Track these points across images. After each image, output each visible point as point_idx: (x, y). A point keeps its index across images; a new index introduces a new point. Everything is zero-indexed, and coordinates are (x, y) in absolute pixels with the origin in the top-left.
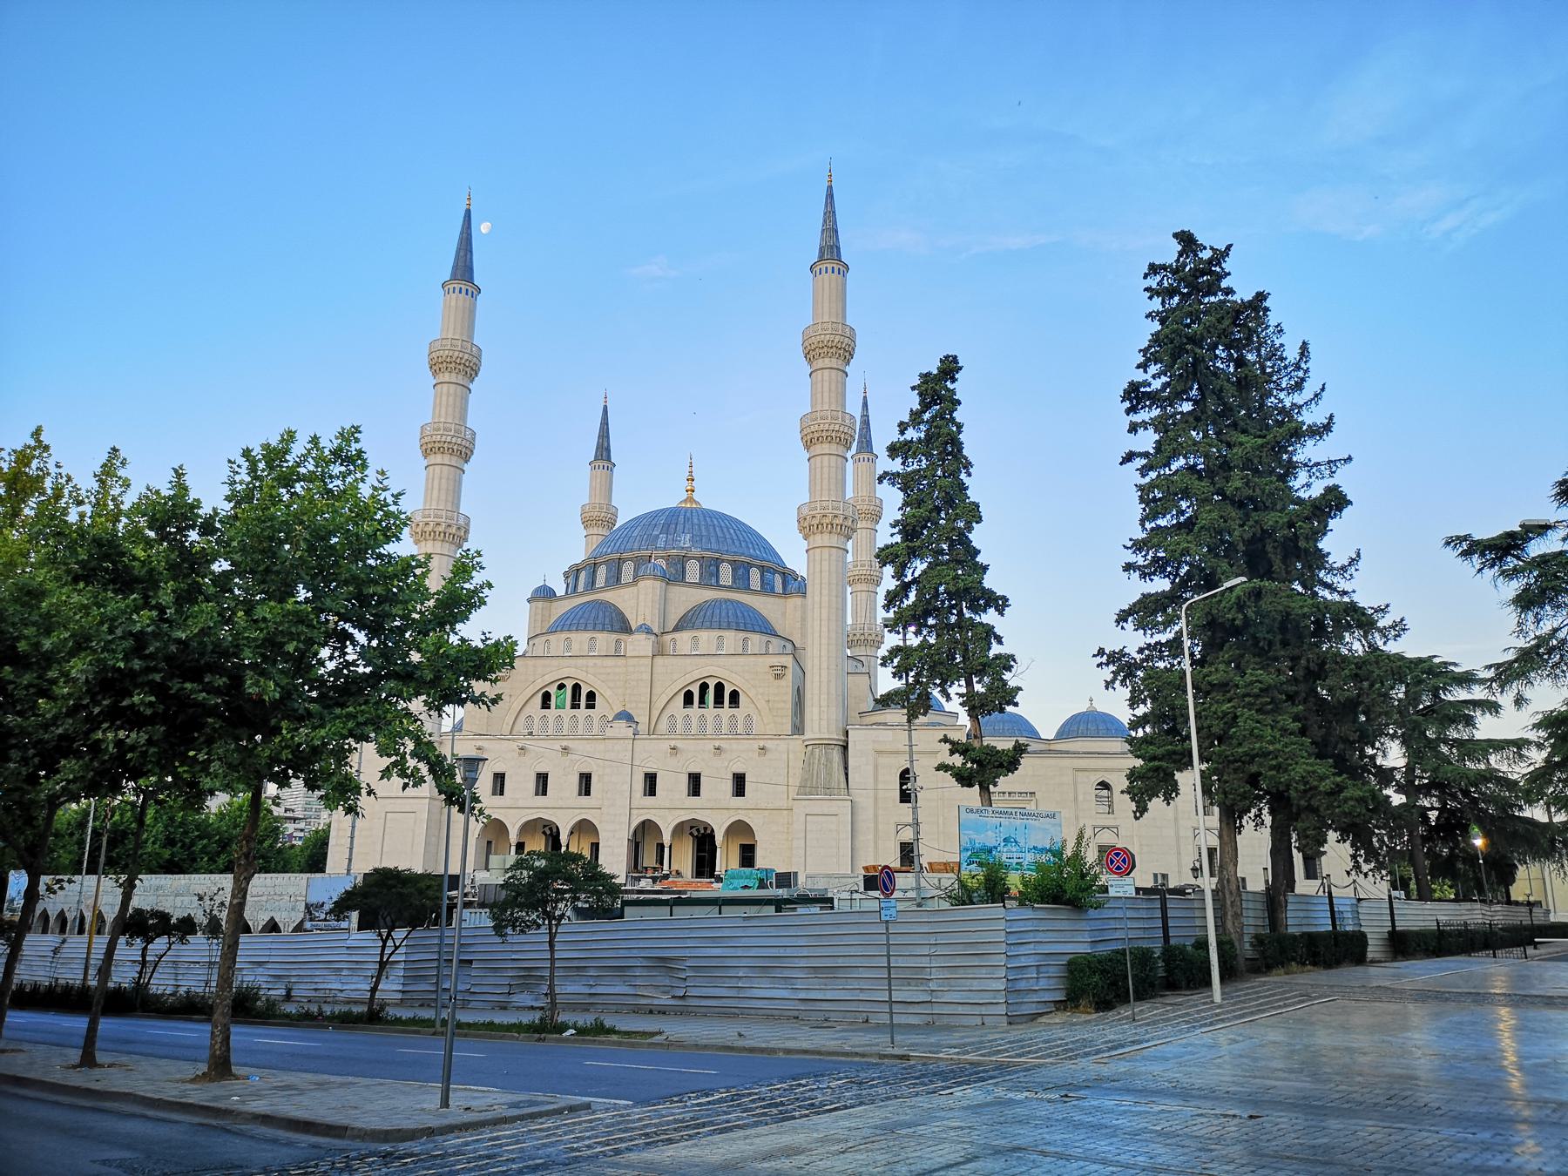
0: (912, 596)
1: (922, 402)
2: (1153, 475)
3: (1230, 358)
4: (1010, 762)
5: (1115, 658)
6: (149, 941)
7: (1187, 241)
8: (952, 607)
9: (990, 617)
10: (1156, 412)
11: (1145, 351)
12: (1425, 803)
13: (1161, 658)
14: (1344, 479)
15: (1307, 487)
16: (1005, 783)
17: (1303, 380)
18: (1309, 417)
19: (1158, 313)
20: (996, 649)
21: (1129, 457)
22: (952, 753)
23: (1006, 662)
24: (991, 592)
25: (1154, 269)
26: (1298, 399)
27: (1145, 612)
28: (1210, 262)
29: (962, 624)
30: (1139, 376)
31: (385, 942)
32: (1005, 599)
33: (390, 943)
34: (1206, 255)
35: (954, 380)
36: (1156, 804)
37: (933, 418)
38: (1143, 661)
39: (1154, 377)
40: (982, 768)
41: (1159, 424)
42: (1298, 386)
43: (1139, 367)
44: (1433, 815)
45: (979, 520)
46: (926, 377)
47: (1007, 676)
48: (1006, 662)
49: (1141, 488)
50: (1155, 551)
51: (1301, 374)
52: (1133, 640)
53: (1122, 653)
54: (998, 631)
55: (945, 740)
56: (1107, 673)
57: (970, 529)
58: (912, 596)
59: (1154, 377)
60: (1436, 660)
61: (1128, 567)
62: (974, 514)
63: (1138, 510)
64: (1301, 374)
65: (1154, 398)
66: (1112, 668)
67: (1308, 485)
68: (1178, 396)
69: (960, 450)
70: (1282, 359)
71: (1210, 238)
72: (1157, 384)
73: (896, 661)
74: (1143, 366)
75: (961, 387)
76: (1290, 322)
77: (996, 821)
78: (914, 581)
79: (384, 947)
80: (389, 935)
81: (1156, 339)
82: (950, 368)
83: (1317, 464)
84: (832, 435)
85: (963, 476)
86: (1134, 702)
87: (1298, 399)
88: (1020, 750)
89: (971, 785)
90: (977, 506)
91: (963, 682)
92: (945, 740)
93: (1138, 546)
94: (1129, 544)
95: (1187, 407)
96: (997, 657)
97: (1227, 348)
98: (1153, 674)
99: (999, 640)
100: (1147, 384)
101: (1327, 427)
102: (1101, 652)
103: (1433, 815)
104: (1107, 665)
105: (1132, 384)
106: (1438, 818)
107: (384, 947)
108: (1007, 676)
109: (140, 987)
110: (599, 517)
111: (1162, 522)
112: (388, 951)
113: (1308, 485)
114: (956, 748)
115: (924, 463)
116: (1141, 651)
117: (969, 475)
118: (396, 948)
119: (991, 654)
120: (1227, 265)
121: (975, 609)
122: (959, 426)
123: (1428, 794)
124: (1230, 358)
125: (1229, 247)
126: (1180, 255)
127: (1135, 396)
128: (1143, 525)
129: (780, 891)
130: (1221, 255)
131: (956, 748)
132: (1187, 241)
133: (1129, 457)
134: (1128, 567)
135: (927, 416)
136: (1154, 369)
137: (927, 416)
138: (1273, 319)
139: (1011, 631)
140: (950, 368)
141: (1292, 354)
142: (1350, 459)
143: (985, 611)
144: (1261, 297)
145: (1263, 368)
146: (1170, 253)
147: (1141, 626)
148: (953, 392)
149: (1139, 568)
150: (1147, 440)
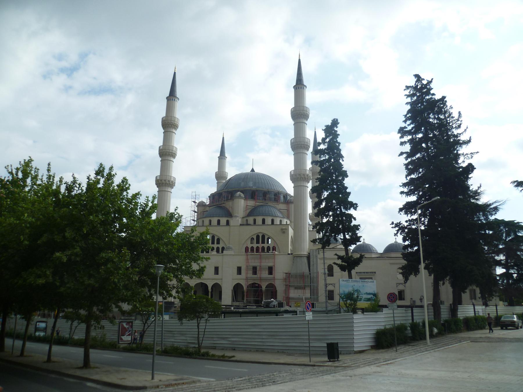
0: (324, 204)
1: (326, 135)
2: (409, 160)
3: (435, 118)
4: (358, 262)
5: (398, 225)
6: (73, 322)
7: (418, 78)
8: (338, 208)
9: (352, 211)
10: (410, 137)
11: (405, 116)
12: (512, 271)
13: (414, 224)
14: (473, 161)
15: (463, 162)
16: (358, 269)
17: (461, 124)
18: (463, 138)
19: (409, 103)
20: (354, 223)
21: (402, 154)
22: (338, 259)
23: (357, 227)
24: (351, 202)
25: (408, 87)
26: (459, 131)
27: (408, 208)
28: (426, 84)
29: (343, 214)
30: (403, 125)
31: (145, 324)
32: (356, 204)
33: (146, 325)
34: (425, 82)
35: (337, 127)
36: (412, 277)
37: (330, 141)
38: (407, 226)
39: (408, 125)
40: (349, 264)
41: (411, 141)
42: (459, 126)
43: (403, 121)
44: (515, 275)
45: (347, 176)
46: (327, 126)
47: (357, 232)
48: (357, 227)
49: (405, 165)
50: (412, 186)
51: (459, 122)
52: (404, 219)
53: (400, 223)
54: (354, 216)
55: (336, 255)
56: (395, 230)
57: (343, 180)
58: (324, 204)
59: (408, 125)
60: (515, 222)
61: (402, 193)
62: (345, 174)
63: (405, 172)
64: (459, 122)
65: (409, 133)
66: (397, 229)
67: (464, 162)
68: (416, 133)
69: (340, 152)
70: (453, 117)
71: (426, 77)
72: (409, 128)
73: (318, 227)
74: (405, 121)
75: (339, 130)
76: (455, 106)
77: (352, 284)
78: (325, 199)
79: (144, 326)
80: (146, 322)
81: (409, 112)
82: (335, 123)
83: (467, 154)
84: (298, 146)
85: (341, 161)
86: (404, 240)
87: (459, 131)
88: (362, 257)
89: (345, 271)
90: (346, 171)
91: (342, 235)
92: (336, 255)
93: (404, 185)
94: (401, 185)
95: (420, 135)
96: (354, 225)
97: (434, 114)
98: (410, 230)
99: (355, 219)
100: (405, 127)
101: (469, 141)
102: (393, 223)
103: (515, 275)
104: (395, 227)
105: (401, 128)
106: (517, 277)
107: (144, 326)
108: (357, 232)
109: (71, 338)
110: (220, 175)
111: (413, 176)
112: (146, 327)
113: (464, 162)
114: (340, 257)
115: (327, 157)
116: (406, 221)
117: (343, 161)
118: (149, 326)
119: (352, 224)
120: (432, 85)
121: (347, 209)
122: (339, 143)
123: (513, 269)
124: (435, 118)
125: (432, 79)
126: (416, 82)
127: (402, 132)
128: (406, 177)
129: (279, 309)
130: (430, 82)
131: (340, 257)
132: (418, 78)
133: (402, 154)
134: (402, 193)
135: (328, 140)
136: (408, 122)
137: (328, 140)
138: (448, 104)
139: (359, 216)
140: (335, 123)
141: (455, 115)
142: (478, 152)
143: (350, 209)
144: (444, 97)
145: (447, 120)
146: (412, 82)
147: (406, 213)
148: (336, 131)
149: (405, 193)
150: (407, 148)
